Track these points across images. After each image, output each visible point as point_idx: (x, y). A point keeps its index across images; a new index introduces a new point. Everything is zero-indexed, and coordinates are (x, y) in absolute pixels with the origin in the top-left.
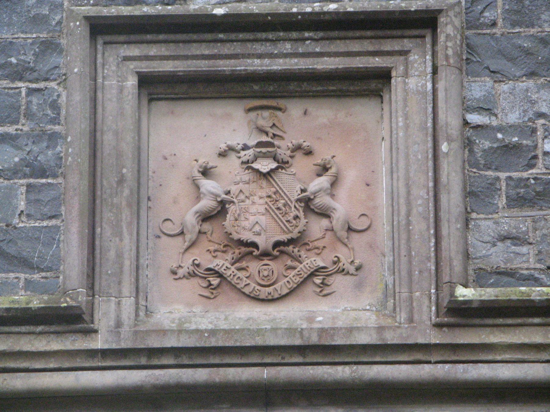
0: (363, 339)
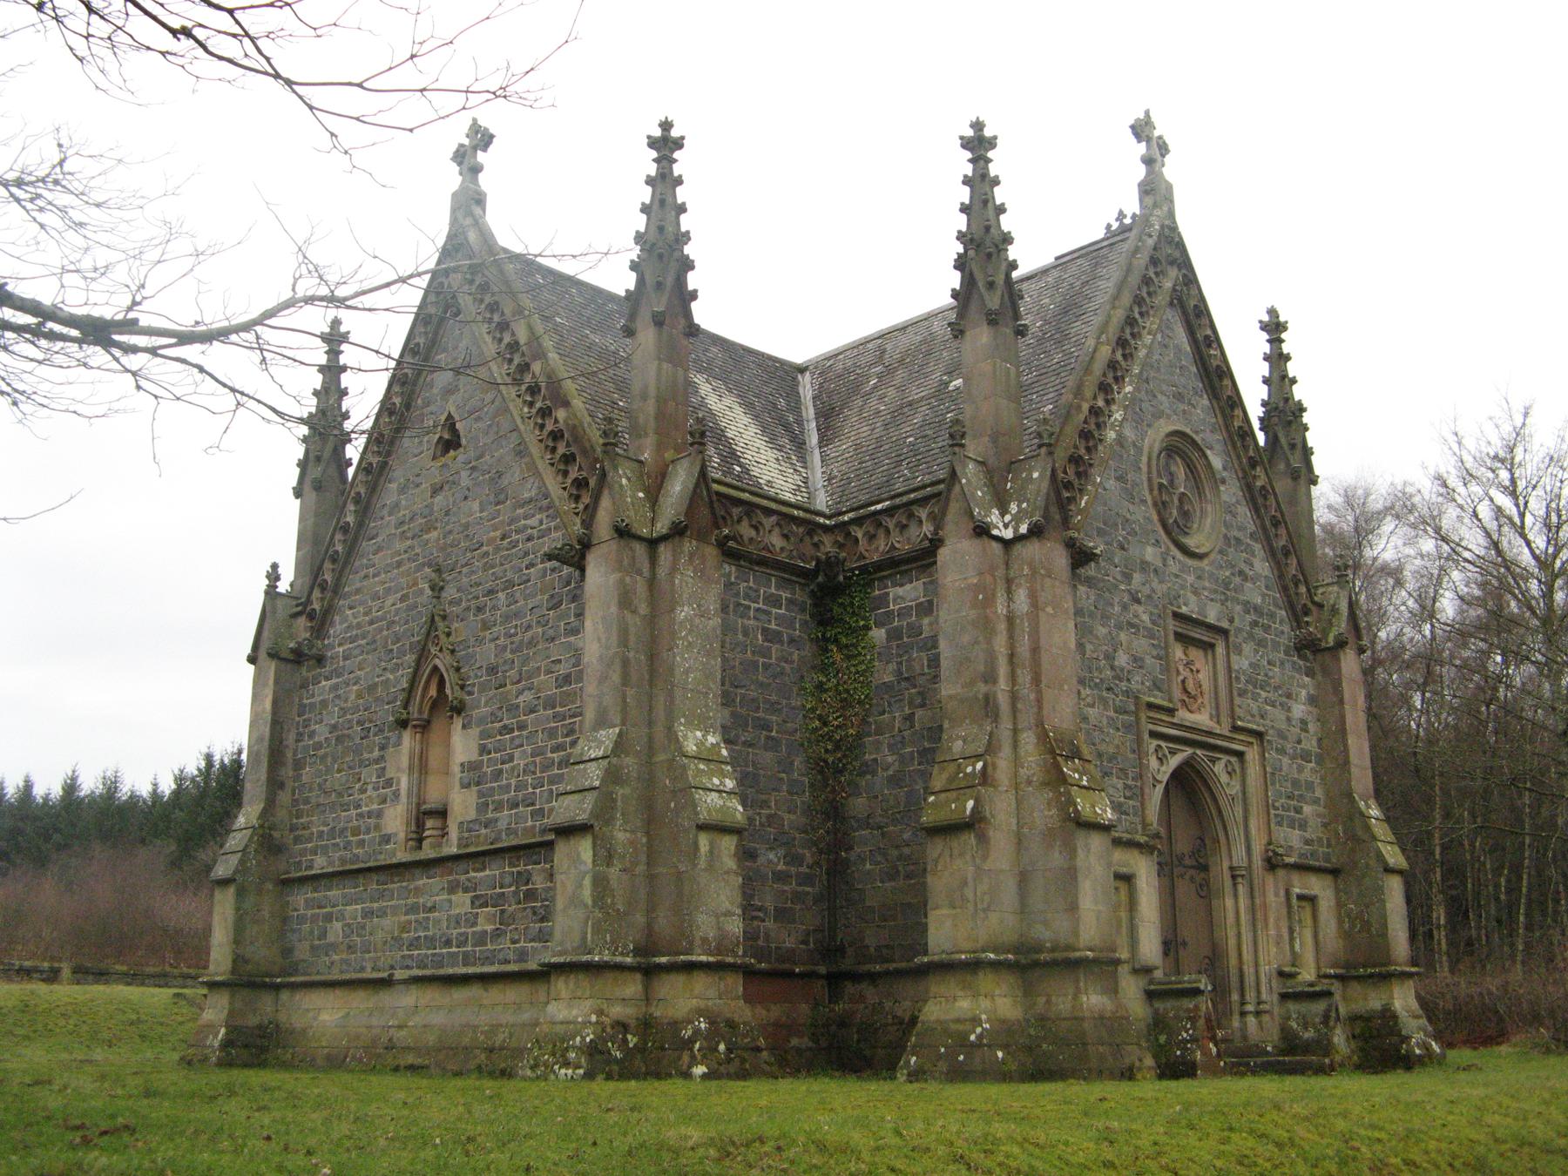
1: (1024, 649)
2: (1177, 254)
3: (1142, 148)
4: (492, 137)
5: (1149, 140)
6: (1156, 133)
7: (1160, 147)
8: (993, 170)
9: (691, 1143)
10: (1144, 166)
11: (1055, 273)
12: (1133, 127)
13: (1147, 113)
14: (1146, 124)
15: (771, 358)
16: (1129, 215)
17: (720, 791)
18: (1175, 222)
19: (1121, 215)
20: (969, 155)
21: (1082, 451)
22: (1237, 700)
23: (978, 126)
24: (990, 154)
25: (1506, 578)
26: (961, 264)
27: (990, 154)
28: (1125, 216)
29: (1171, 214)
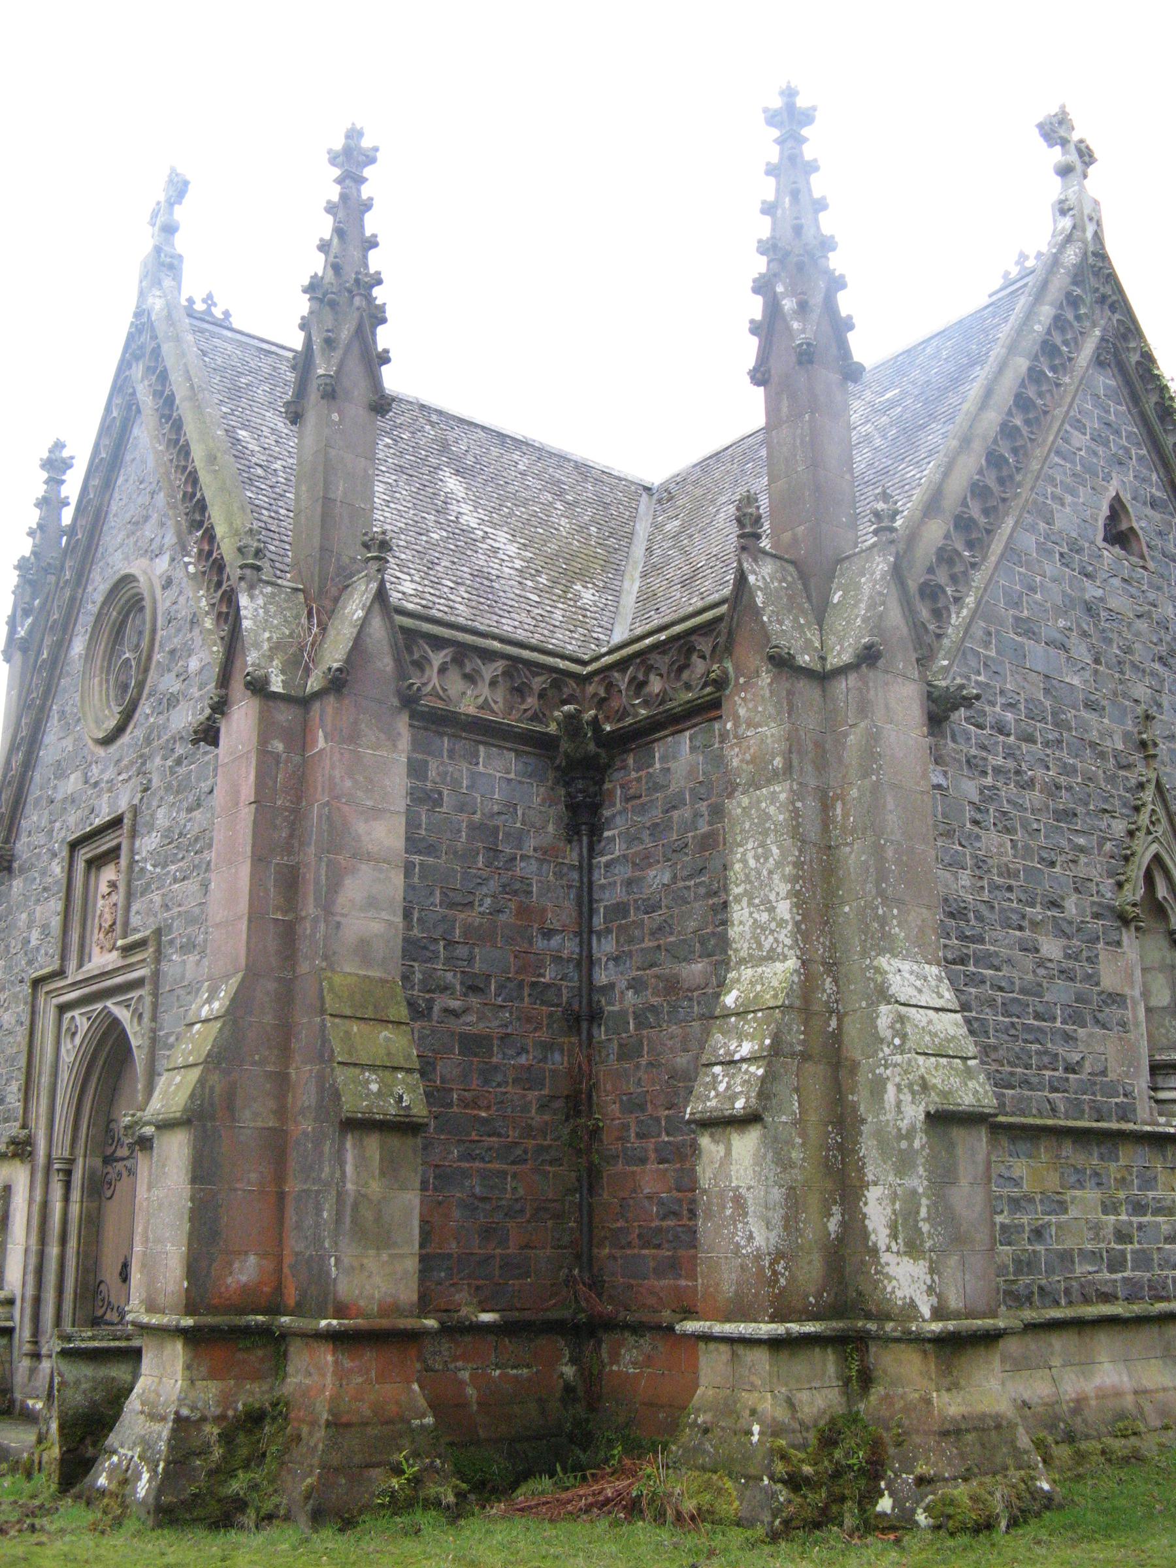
0: (110, 968)
1: (516, 598)
2: (1108, 290)
3: (1056, 155)
4: (186, 183)
5: (1064, 142)
6: (1075, 136)
7: (1081, 154)
8: (809, 152)
9: (88, 1441)
10: (1059, 179)
11: (934, 343)
12: (1040, 126)
13: (1063, 107)
14: (1061, 123)
15: (583, 470)
16: (1032, 254)
17: (130, 896)
18: (1103, 248)
19: (1023, 257)
20: (775, 133)
21: (959, 546)
22: (1052, 455)
23: (790, 94)
24: (805, 132)
25: (507, 1375)
26: (762, 286)
27: (805, 132)
28: (1027, 258)
29: (1098, 237)
